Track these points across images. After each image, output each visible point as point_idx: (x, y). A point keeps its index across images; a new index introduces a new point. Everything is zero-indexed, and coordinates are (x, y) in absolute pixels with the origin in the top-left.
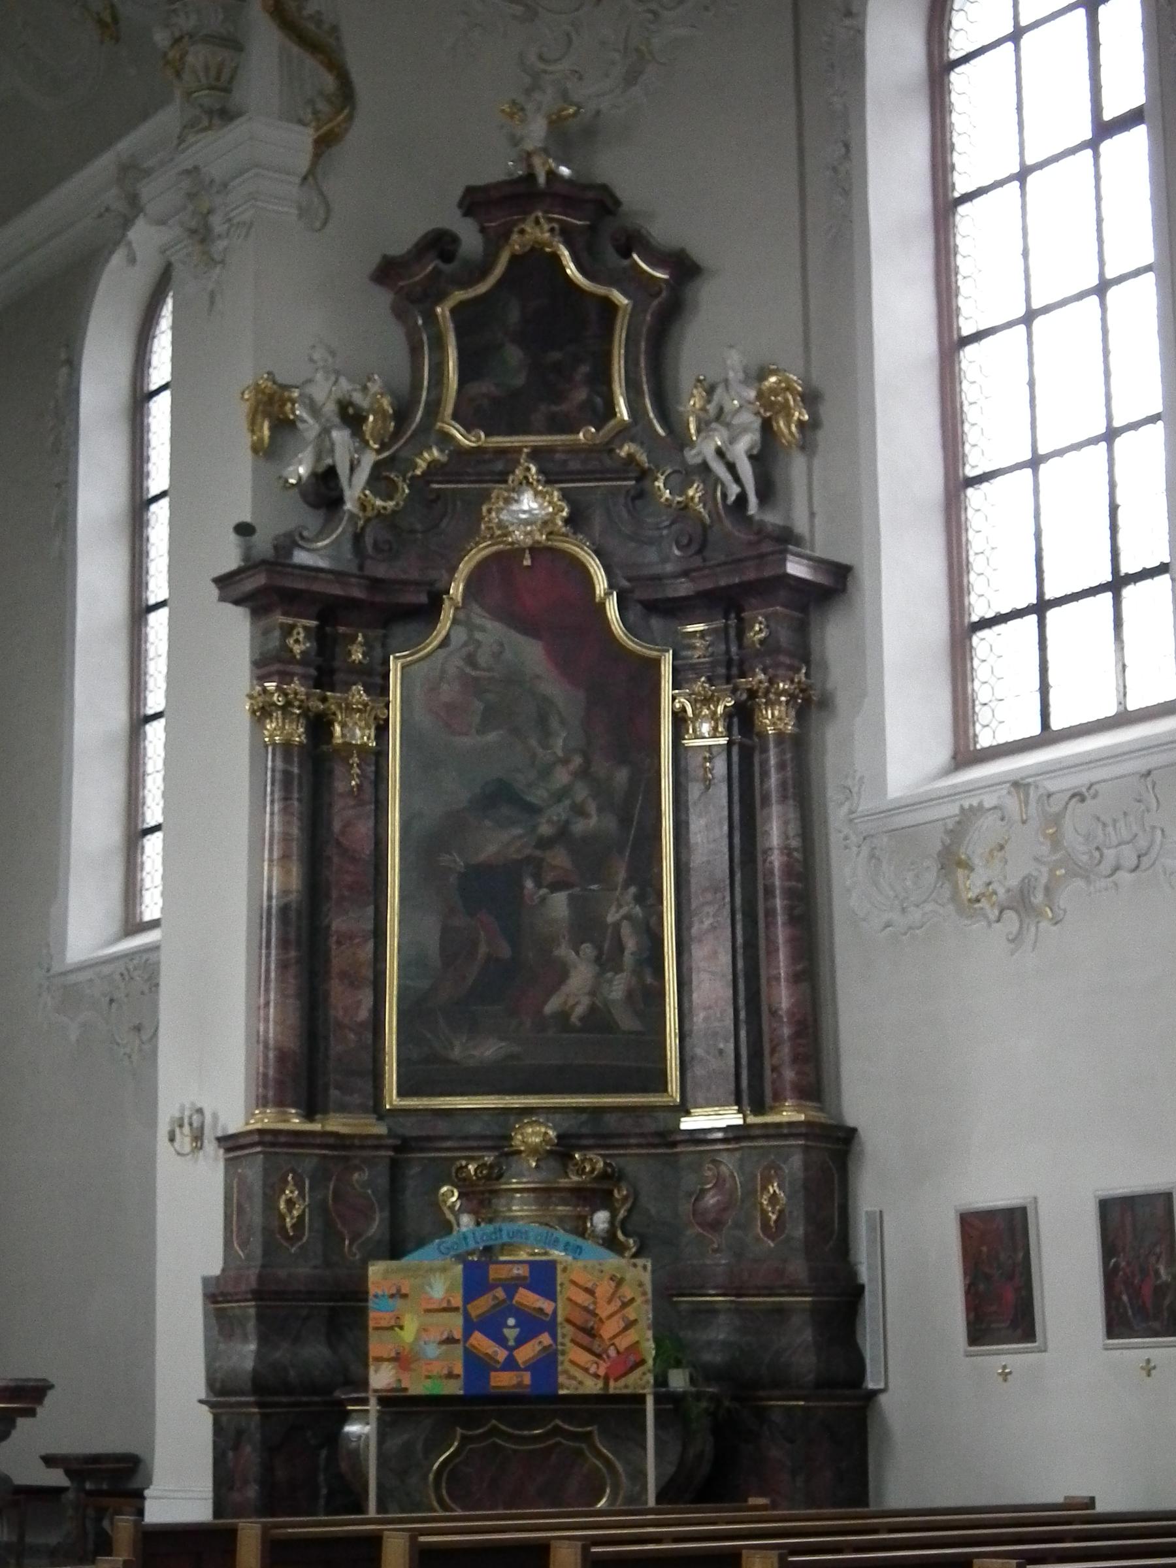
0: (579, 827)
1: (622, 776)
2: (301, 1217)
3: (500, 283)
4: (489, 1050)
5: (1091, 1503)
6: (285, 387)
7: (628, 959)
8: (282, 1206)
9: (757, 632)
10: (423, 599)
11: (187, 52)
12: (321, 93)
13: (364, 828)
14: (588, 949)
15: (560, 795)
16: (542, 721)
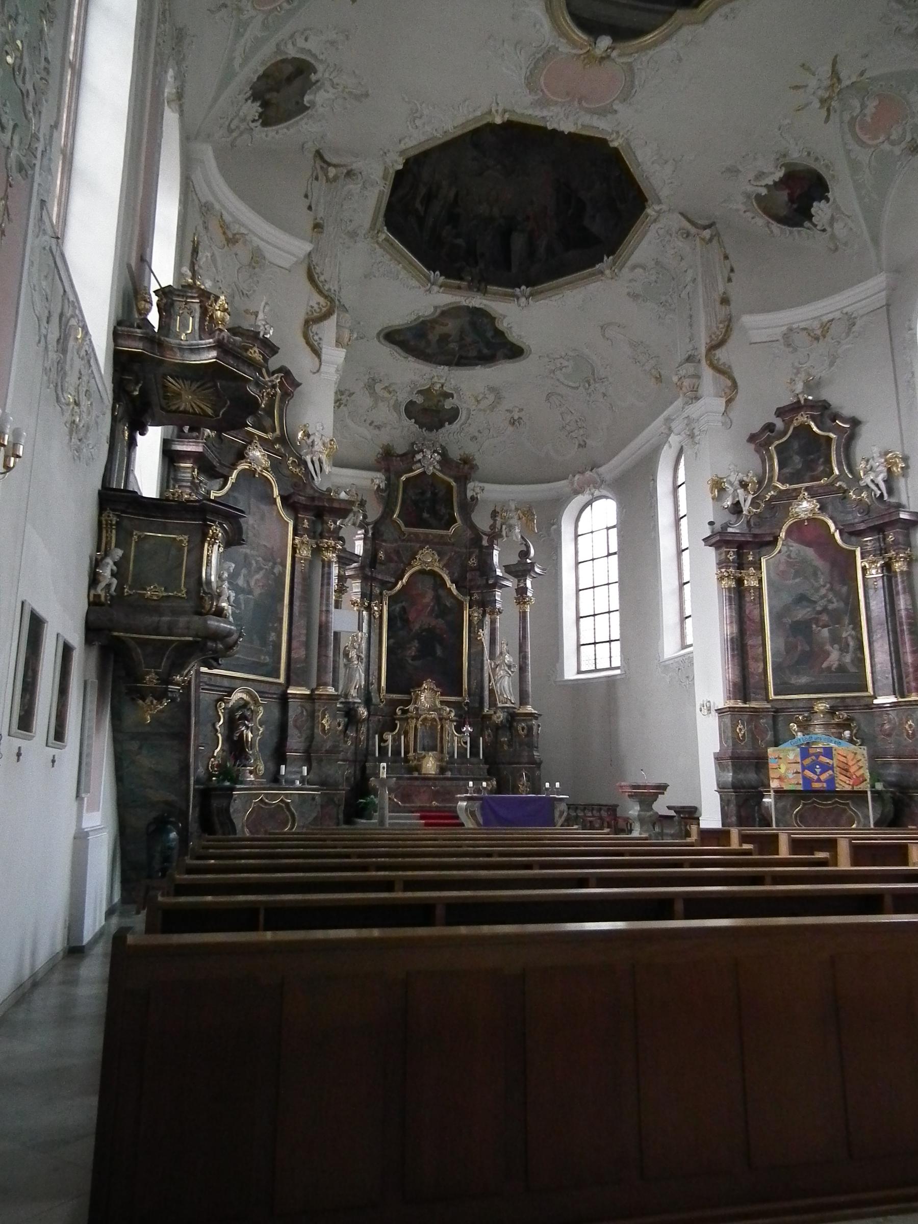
1: (844, 589)
2: (744, 734)
4: (804, 680)
7: (851, 648)
9: (891, 538)
13: (756, 612)
15: (822, 597)
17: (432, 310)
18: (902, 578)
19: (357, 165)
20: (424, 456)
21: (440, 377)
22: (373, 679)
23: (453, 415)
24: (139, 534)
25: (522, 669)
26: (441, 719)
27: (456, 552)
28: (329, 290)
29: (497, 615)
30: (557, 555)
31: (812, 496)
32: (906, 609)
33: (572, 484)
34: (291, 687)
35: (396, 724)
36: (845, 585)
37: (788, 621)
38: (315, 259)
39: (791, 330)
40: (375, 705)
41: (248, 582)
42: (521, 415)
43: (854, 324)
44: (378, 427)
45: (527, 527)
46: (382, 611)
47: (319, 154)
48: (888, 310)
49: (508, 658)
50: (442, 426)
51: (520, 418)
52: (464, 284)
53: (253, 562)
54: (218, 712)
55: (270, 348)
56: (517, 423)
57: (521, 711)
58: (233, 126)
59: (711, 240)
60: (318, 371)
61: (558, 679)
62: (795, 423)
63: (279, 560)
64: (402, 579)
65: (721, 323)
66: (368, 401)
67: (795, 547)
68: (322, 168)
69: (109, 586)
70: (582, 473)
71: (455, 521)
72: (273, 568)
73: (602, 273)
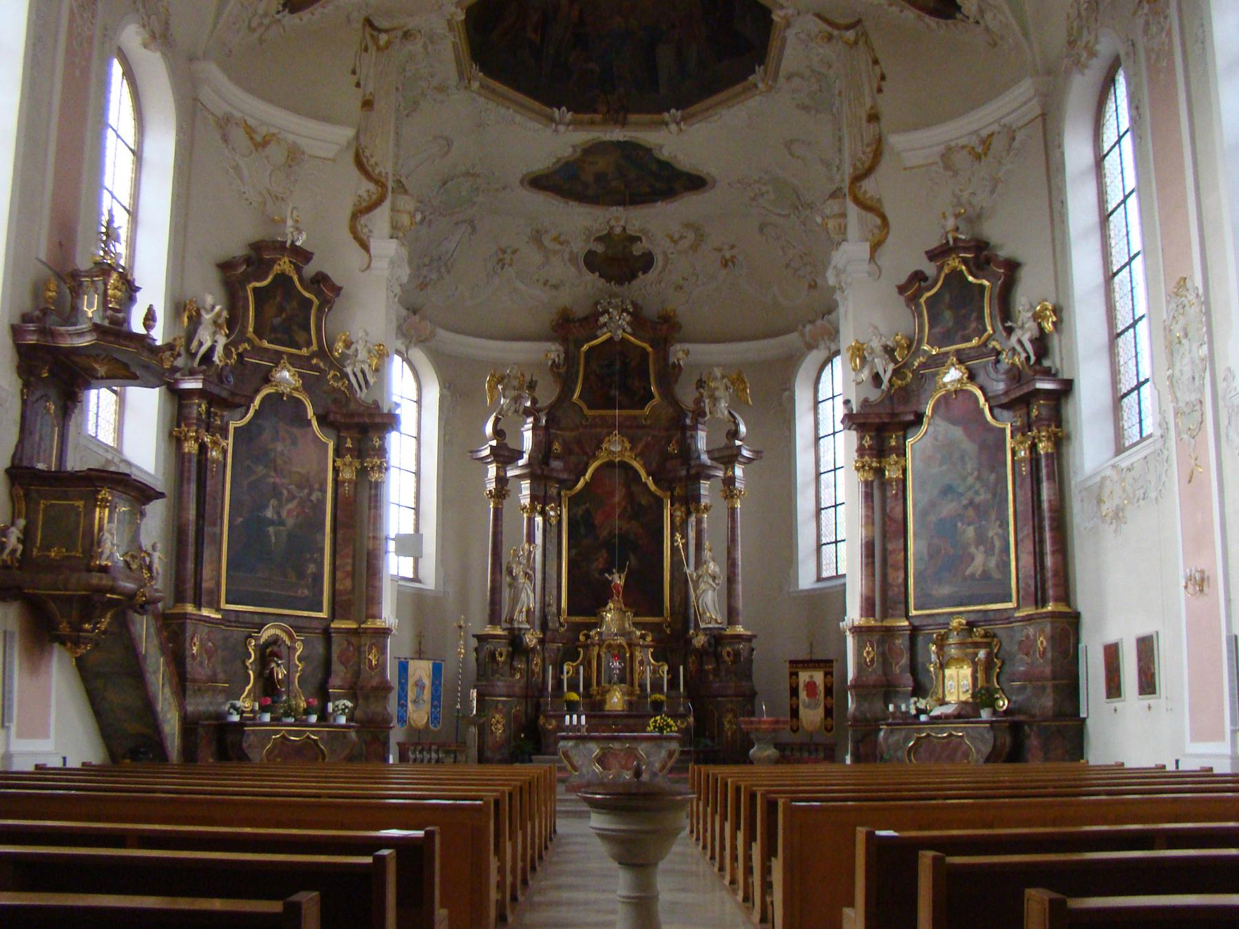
0: (978, 499)
1: (992, 477)
2: (873, 659)
3: (941, 287)
4: (946, 590)
5: (1211, 769)
6: (863, 344)
7: (997, 551)
8: (865, 654)
9: (1035, 412)
10: (911, 417)
11: (372, 687)
12: (875, 227)
13: (899, 509)
14: (982, 548)
15: (970, 488)
16: (962, 458)
17: (571, 150)
18: (1047, 460)
19: (411, 23)
20: (610, 318)
21: (618, 219)
22: (552, 600)
23: (647, 262)
24: (45, 502)
25: (731, 580)
26: (630, 645)
27: (653, 437)
28: (380, 173)
29: (703, 512)
30: (790, 430)
31: (961, 362)
32: (1050, 501)
33: (803, 335)
34: (336, 621)
35: (579, 653)
36: (992, 472)
37: (932, 518)
38: (364, 141)
39: (949, 149)
40: (553, 631)
41: (278, 513)
42: (734, 252)
43: (1014, 139)
44: (556, 287)
45: (737, 402)
46: (560, 516)
47: (369, 22)
48: (1044, 121)
49: (712, 567)
50: (634, 276)
51: (733, 257)
52: (598, 117)
53: (285, 492)
54: (248, 649)
55: (301, 255)
56: (730, 264)
57: (729, 632)
58: (254, 24)
59: (856, 43)
60: (369, 266)
61: (791, 590)
62: (946, 270)
63: (317, 486)
64: (584, 474)
65: (868, 145)
66: (536, 258)
67: (942, 426)
68: (372, 36)
69: (14, 551)
70: (812, 322)
71: (652, 397)
72: (310, 494)
73: (756, 86)
